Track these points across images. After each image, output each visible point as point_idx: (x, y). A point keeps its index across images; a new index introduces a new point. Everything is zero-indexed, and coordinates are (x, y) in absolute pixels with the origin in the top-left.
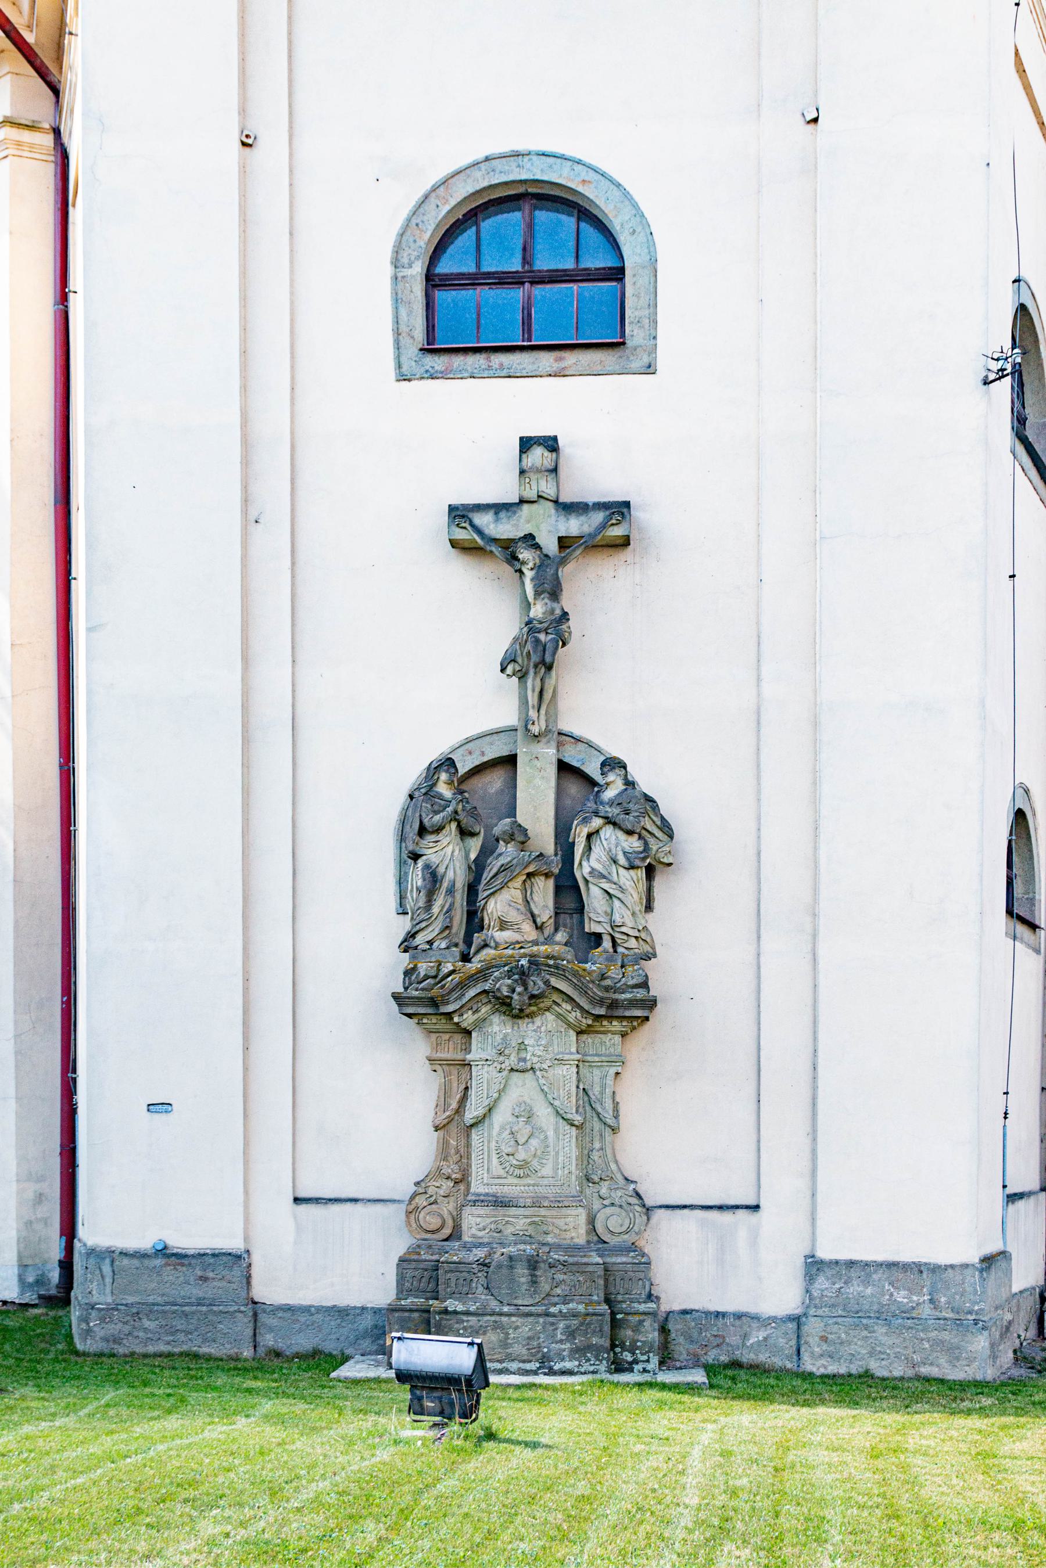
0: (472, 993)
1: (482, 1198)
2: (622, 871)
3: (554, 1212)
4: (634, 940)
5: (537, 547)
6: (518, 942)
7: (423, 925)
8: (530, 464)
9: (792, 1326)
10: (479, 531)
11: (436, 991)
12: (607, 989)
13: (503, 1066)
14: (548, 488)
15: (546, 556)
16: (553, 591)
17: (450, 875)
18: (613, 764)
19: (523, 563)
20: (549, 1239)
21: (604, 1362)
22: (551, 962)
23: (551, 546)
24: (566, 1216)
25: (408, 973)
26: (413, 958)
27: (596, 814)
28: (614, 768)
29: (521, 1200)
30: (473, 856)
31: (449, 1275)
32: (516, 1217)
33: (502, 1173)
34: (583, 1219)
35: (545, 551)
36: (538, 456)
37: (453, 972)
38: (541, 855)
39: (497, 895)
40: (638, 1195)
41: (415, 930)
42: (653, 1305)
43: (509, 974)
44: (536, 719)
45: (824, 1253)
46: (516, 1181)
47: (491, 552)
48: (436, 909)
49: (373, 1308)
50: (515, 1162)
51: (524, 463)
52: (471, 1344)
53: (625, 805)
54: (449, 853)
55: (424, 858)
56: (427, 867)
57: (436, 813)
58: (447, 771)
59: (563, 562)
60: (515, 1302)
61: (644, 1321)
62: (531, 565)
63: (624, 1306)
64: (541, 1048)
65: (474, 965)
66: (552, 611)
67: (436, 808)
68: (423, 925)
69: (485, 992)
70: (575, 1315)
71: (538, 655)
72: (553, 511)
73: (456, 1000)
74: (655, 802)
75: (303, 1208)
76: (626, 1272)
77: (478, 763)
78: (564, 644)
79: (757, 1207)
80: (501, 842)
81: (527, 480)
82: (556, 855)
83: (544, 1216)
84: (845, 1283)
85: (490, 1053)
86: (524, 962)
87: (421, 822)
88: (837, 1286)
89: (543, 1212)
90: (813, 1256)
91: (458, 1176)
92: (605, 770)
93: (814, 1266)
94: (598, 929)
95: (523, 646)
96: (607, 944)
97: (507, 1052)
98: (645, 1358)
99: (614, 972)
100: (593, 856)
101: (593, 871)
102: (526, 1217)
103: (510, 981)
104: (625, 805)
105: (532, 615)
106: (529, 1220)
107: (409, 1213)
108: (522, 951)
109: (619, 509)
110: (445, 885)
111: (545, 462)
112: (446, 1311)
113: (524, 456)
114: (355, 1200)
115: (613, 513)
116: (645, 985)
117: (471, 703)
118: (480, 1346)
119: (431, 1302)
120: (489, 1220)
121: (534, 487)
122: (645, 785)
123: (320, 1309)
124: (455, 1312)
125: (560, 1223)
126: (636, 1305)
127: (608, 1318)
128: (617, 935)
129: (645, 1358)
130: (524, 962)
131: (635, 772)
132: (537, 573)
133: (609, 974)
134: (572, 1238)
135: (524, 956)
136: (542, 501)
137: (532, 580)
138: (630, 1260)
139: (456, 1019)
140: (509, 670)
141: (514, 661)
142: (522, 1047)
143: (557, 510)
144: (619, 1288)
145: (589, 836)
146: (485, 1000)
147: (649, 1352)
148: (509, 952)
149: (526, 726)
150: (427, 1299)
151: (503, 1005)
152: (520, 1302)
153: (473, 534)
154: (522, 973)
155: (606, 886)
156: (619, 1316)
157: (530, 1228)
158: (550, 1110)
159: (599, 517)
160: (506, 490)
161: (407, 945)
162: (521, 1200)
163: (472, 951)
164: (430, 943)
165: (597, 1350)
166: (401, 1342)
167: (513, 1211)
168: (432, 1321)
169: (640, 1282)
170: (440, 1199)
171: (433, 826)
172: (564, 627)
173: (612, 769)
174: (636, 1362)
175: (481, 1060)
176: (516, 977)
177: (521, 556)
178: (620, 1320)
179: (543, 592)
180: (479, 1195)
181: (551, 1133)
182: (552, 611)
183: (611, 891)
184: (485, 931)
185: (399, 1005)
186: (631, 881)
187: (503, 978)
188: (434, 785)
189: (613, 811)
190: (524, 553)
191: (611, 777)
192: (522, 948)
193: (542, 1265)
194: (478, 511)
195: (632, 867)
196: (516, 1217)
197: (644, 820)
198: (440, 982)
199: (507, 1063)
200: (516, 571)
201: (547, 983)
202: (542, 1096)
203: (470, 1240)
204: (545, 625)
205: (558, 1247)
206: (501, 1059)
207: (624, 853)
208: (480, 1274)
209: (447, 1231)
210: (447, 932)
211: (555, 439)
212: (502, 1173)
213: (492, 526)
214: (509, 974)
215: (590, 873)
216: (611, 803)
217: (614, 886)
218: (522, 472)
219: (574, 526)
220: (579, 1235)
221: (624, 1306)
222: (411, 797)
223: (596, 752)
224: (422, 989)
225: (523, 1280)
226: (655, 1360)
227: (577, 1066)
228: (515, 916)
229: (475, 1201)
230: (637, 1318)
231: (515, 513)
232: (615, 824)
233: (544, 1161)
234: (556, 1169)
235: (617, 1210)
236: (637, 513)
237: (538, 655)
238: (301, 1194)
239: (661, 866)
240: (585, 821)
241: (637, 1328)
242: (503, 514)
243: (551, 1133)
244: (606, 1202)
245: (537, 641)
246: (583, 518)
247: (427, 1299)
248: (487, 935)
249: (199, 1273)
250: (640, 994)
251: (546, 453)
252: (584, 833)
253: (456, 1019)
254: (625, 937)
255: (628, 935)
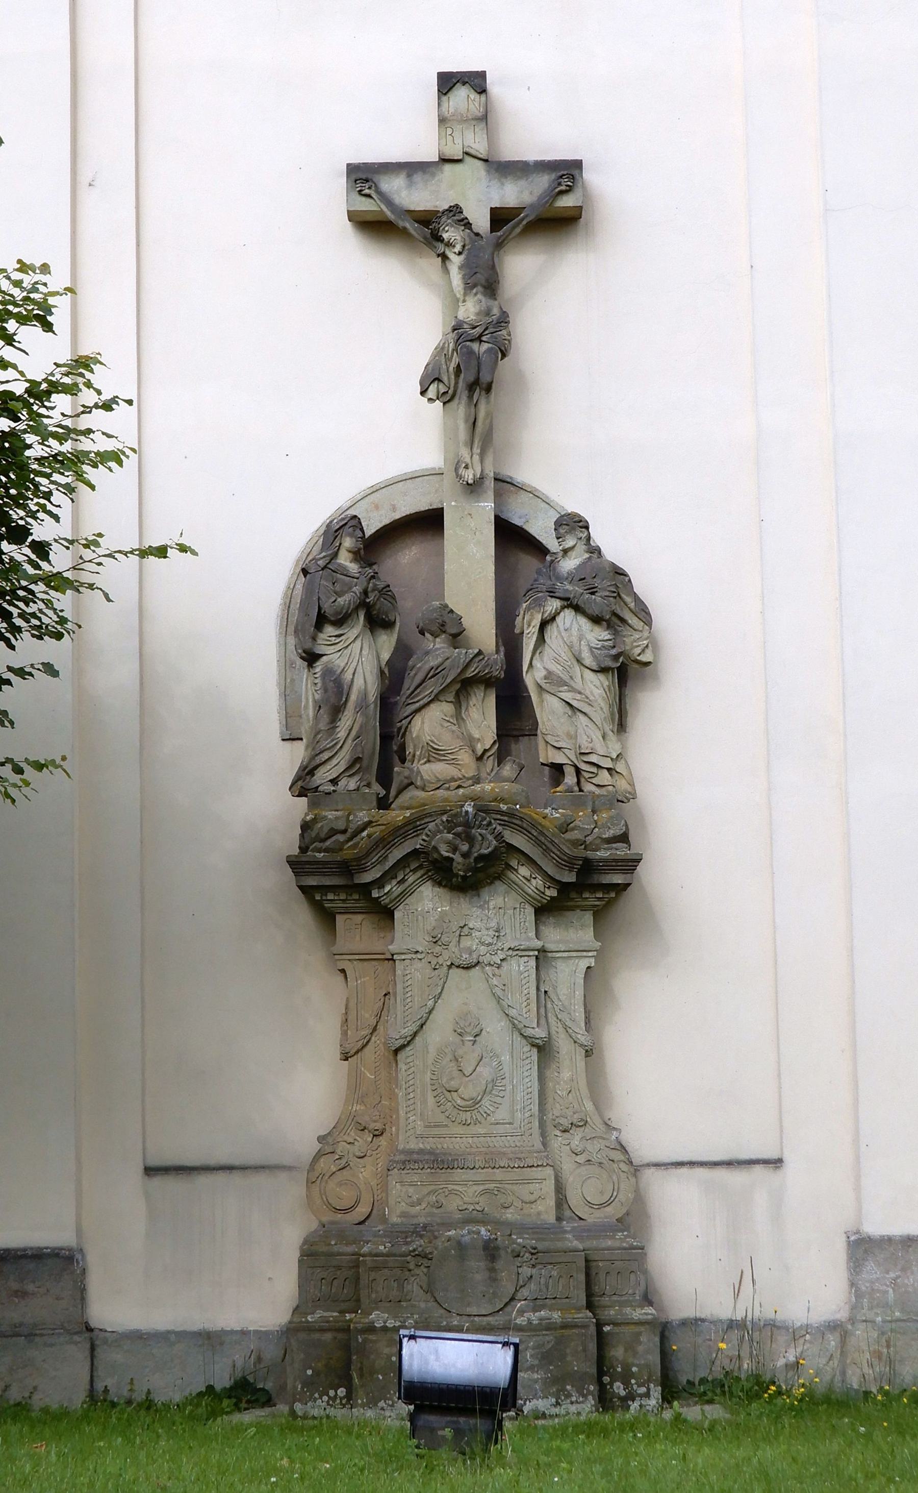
0: (397, 854)
1: (415, 1156)
2: (589, 675)
3: (516, 1174)
4: (606, 772)
5: (468, 225)
6: (453, 779)
7: (326, 756)
8: (452, 110)
9: (832, 1341)
10: (389, 202)
11: (348, 853)
12: (576, 843)
13: (440, 960)
14: (479, 145)
15: (477, 234)
16: (485, 280)
17: (359, 683)
18: (573, 524)
19: (449, 245)
20: (510, 1215)
21: (590, 1397)
22: (504, 807)
23: (481, 221)
24: (529, 1181)
25: (306, 827)
26: (312, 805)
27: (552, 593)
28: (573, 529)
29: (470, 1158)
30: (386, 656)
31: (373, 1275)
32: (465, 1183)
33: (442, 1118)
34: (549, 1187)
35: (475, 228)
36: (462, 96)
37: (369, 824)
38: (480, 653)
39: (423, 712)
40: (623, 1149)
41: (314, 764)
42: (650, 1310)
43: (450, 826)
44: (468, 460)
45: (875, 1227)
46: (460, 1130)
47: (405, 228)
48: (342, 734)
49: (256, 1332)
50: (459, 1101)
51: (445, 105)
52: (505, 1344)
53: (590, 581)
54: (358, 658)
55: (324, 659)
56: (328, 672)
57: (339, 594)
58: (351, 535)
59: (499, 245)
60: (469, 1310)
61: (640, 1334)
62: (458, 248)
63: (612, 1312)
64: (491, 933)
65: (397, 815)
66: (488, 313)
67: (338, 587)
68: (326, 756)
69: (415, 853)
70: (550, 1327)
71: (473, 372)
72: (483, 173)
73: (379, 862)
74: (626, 575)
75: (157, 1182)
76: (612, 1261)
77: (386, 521)
78: (504, 355)
79: (777, 1163)
80: (427, 635)
81: (449, 131)
82: (497, 652)
83: (500, 1182)
84: (903, 1269)
85: (421, 943)
86: (469, 808)
87: (320, 608)
88: (892, 1275)
89: (499, 1174)
90: (858, 1232)
91: (378, 1126)
92: (562, 531)
93: (862, 1248)
94: (559, 759)
95: (448, 359)
96: (570, 779)
97: (445, 939)
98: (643, 1390)
99: (582, 818)
100: (547, 651)
101: (549, 675)
102: (476, 1183)
103: (450, 836)
104: (590, 581)
105: (461, 315)
106: (482, 1188)
107: (310, 1183)
108: (461, 791)
109: (567, 173)
110: (353, 697)
111: (471, 106)
112: (371, 1329)
113: (445, 98)
114: (230, 1168)
115: (561, 177)
116: (624, 838)
117: (382, 438)
118: (516, 1346)
119: (348, 1316)
120: (426, 1190)
121: (458, 141)
122: (613, 553)
123: (182, 1335)
124: (385, 1329)
125: (524, 1191)
126: (628, 1310)
127: (593, 1329)
128: (583, 766)
129: (643, 1390)
130: (469, 808)
131: (598, 536)
132: (467, 259)
133: (577, 823)
134: (539, 1214)
135: (466, 798)
136: (468, 159)
137: (460, 268)
138: (617, 1244)
139: (375, 894)
140: (432, 392)
141: (438, 380)
142: (463, 931)
143: (488, 172)
144: (605, 1284)
145: (544, 625)
146: (414, 865)
147: (649, 1381)
148: (441, 792)
149: (456, 470)
150: (342, 1312)
151: (442, 873)
152: (473, 1310)
153: (387, 214)
154: (467, 825)
155: (568, 696)
156: (607, 1329)
157: (482, 1199)
158: (504, 1023)
159: (543, 182)
160: (424, 145)
161: (303, 784)
162: (470, 1158)
163: (393, 792)
164: (334, 782)
165: (579, 1381)
166: (412, 1342)
167: (459, 1175)
168: (354, 1344)
169: (632, 1276)
170: (354, 1162)
171: (337, 613)
172: (504, 332)
173: (571, 530)
174: (631, 1397)
175: (409, 951)
176: (460, 829)
177: (445, 236)
178: (608, 1333)
179: (475, 286)
180: (411, 1152)
181: (506, 1058)
182: (488, 313)
183: (574, 703)
184: (407, 764)
185: (296, 874)
186: (596, 687)
187: (440, 832)
188: (336, 555)
189: (570, 588)
190: (451, 233)
191: (570, 542)
192: (459, 787)
193: (502, 1253)
194: (385, 173)
195: (603, 670)
196: (465, 1183)
197: (610, 600)
198: (350, 839)
199: (446, 955)
200: (439, 256)
201: (499, 837)
202: (493, 1003)
203: (399, 1220)
204: (478, 330)
205: (522, 1228)
206: (438, 949)
207: (591, 648)
208: (417, 1271)
209: (362, 1210)
210: (358, 766)
211: (482, 75)
212: (442, 1118)
213: (404, 193)
214: (450, 826)
215: (546, 678)
216: (571, 578)
217: (578, 697)
218: (442, 121)
219: (511, 194)
220: (546, 1209)
221: (612, 1312)
222: (305, 572)
223: (543, 505)
224: (326, 850)
225: (478, 1277)
226: (656, 1392)
227: (537, 957)
228: (450, 739)
229: (404, 1162)
230: (633, 1329)
231: (433, 175)
232: (577, 609)
233: (498, 1100)
234: (513, 1112)
235: (595, 1169)
236: (589, 175)
237: (473, 372)
238: (154, 1162)
239: (636, 666)
240: (539, 604)
241: (630, 1348)
242: (418, 177)
243: (506, 1058)
244: (581, 1159)
245: (471, 352)
246: (522, 183)
247: (342, 1312)
248: (411, 770)
249: (14, 1286)
250: (620, 851)
251: (473, 95)
252: (537, 622)
253: (375, 894)
254: (594, 770)
255: (598, 766)
